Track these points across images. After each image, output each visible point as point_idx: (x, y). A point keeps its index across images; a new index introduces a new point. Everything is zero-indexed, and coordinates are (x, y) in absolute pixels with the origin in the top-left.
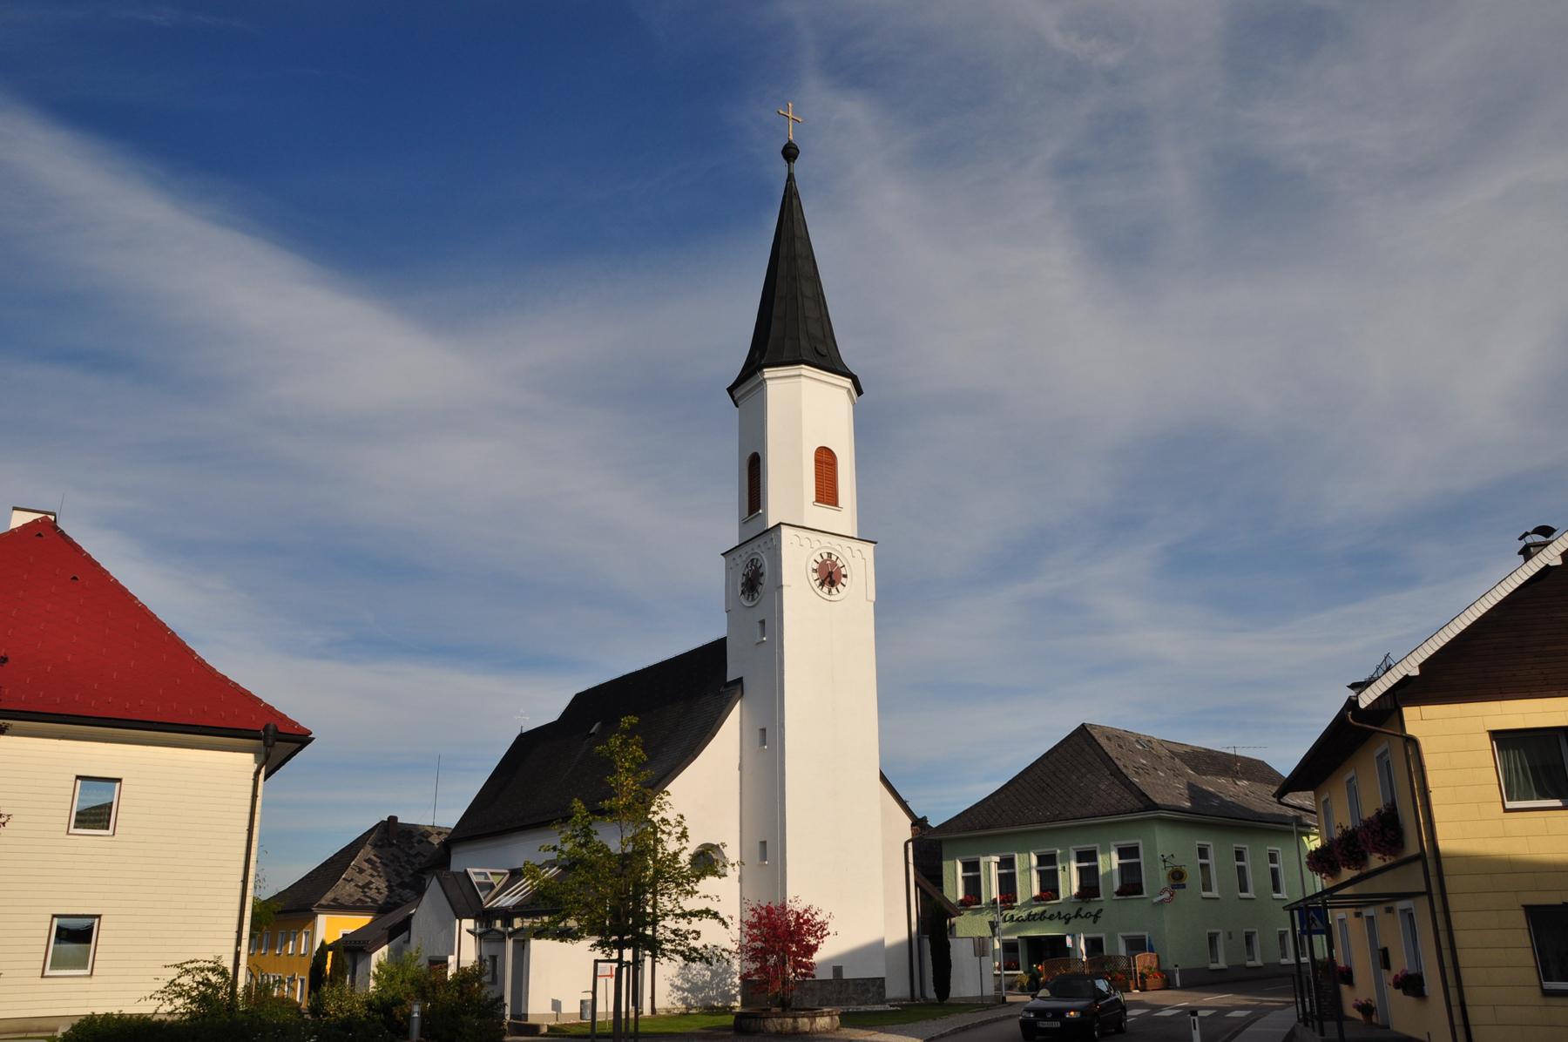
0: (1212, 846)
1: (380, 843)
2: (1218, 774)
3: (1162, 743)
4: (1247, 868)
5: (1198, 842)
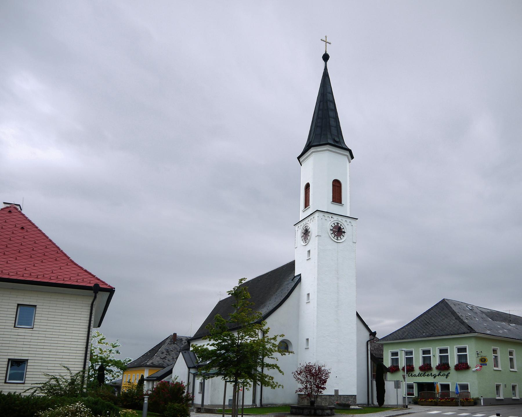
0: (499, 349)
1: (170, 343)
2: (502, 321)
3: (477, 307)
4: (514, 359)
5: (493, 347)
